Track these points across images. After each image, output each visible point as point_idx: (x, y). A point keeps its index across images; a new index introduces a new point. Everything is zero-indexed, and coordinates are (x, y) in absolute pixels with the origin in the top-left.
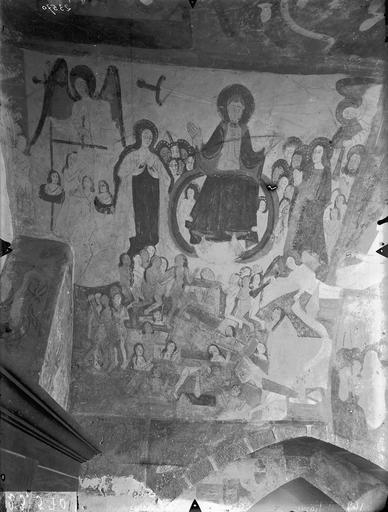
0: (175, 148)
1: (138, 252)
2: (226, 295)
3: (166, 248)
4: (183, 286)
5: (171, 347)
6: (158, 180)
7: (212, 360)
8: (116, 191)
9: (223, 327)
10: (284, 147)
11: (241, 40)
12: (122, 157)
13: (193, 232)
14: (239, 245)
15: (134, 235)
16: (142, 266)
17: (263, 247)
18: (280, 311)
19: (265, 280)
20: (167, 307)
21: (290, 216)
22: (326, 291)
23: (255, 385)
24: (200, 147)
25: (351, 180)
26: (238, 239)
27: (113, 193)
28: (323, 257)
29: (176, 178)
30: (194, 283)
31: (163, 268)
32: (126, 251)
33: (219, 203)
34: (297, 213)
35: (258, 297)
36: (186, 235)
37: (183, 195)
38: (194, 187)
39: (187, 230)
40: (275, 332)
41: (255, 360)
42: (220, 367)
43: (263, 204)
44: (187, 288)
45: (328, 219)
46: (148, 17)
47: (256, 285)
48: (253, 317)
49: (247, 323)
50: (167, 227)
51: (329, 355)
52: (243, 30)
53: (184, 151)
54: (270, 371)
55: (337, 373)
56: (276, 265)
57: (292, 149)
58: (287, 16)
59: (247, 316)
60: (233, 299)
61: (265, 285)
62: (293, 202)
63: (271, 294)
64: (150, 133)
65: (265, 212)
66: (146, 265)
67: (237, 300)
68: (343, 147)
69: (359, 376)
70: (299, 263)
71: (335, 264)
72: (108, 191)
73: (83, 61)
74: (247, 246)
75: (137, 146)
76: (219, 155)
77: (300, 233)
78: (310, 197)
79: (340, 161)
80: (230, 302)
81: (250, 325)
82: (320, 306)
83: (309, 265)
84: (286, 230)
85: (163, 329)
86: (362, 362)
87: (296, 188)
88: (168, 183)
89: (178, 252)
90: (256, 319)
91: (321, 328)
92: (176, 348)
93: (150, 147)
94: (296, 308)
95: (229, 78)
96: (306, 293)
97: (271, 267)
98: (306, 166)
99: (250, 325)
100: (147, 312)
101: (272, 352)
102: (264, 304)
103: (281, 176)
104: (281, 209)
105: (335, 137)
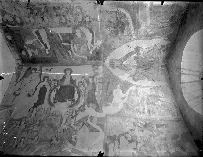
0: (53, 81)
1: (36, 107)
2: (63, 118)
3: (46, 105)
4: (48, 117)
5: (36, 138)
6: (47, 88)
7: (52, 142)
8: (35, 91)
9: (59, 130)
10: (81, 79)
11: (68, 60)
12: (39, 84)
13: (55, 100)
14: (69, 103)
15: (36, 102)
16: (36, 111)
17: (76, 103)
18: (82, 123)
19: (77, 113)
20: (41, 124)
21: (85, 94)
22: (99, 115)
23: (68, 152)
24: (59, 80)
25: (101, 84)
26: (69, 101)
27: (34, 92)
28: (97, 105)
29: (52, 87)
30: (52, 115)
31: (43, 111)
32: (32, 107)
33: (63, 92)
34: (87, 93)
35: (75, 118)
36: (52, 101)
37: (53, 91)
38: (57, 89)
39: (53, 100)
40: (80, 131)
41: (71, 142)
42: (55, 145)
43: (76, 92)
44: (49, 117)
45: (97, 94)
46: (48, 56)
47: (74, 115)
48: (72, 125)
49: (69, 127)
50: (47, 99)
51: (103, 139)
52: (67, 57)
53: (55, 81)
54: (76, 146)
55: (108, 146)
56: (81, 108)
57: (83, 79)
58: (74, 53)
59: (70, 125)
60: (65, 120)
61: (77, 114)
62: (85, 91)
63: (79, 118)
64: (47, 78)
65: (77, 94)
66: (38, 111)
67: (67, 120)
68: (97, 78)
69: (118, 147)
70: (89, 107)
71: (101, 106)
72: (33, 92)
73: (36, 67)
74: (71, 103)
75: (43, 81)
76: (64, 81)
77: (88, 98)
78: (90, 89)
79: (97, 81)
80: (64, 121)
81: (71, 128)
82: (98, 120)
83: (92, 107)
84: (84, 98)
85: (36, 131)
86: (119, 141)
87: (86, 87)
88: (50, 88)
89: (49, 106)
90: (74, 126)
91: (98, 128)
92: (38, 138)
93: (47, 81)
94: (89, 121)
95: (66, 67)
96: (92, 116)
97: (79, 109)
98: (88, 82)
99: (71, 128)
100: (32, 126)
101: (79, 138)
102: (77, 120)
103: (81, 85)
104: (82, 93)
105: (94, 76)
